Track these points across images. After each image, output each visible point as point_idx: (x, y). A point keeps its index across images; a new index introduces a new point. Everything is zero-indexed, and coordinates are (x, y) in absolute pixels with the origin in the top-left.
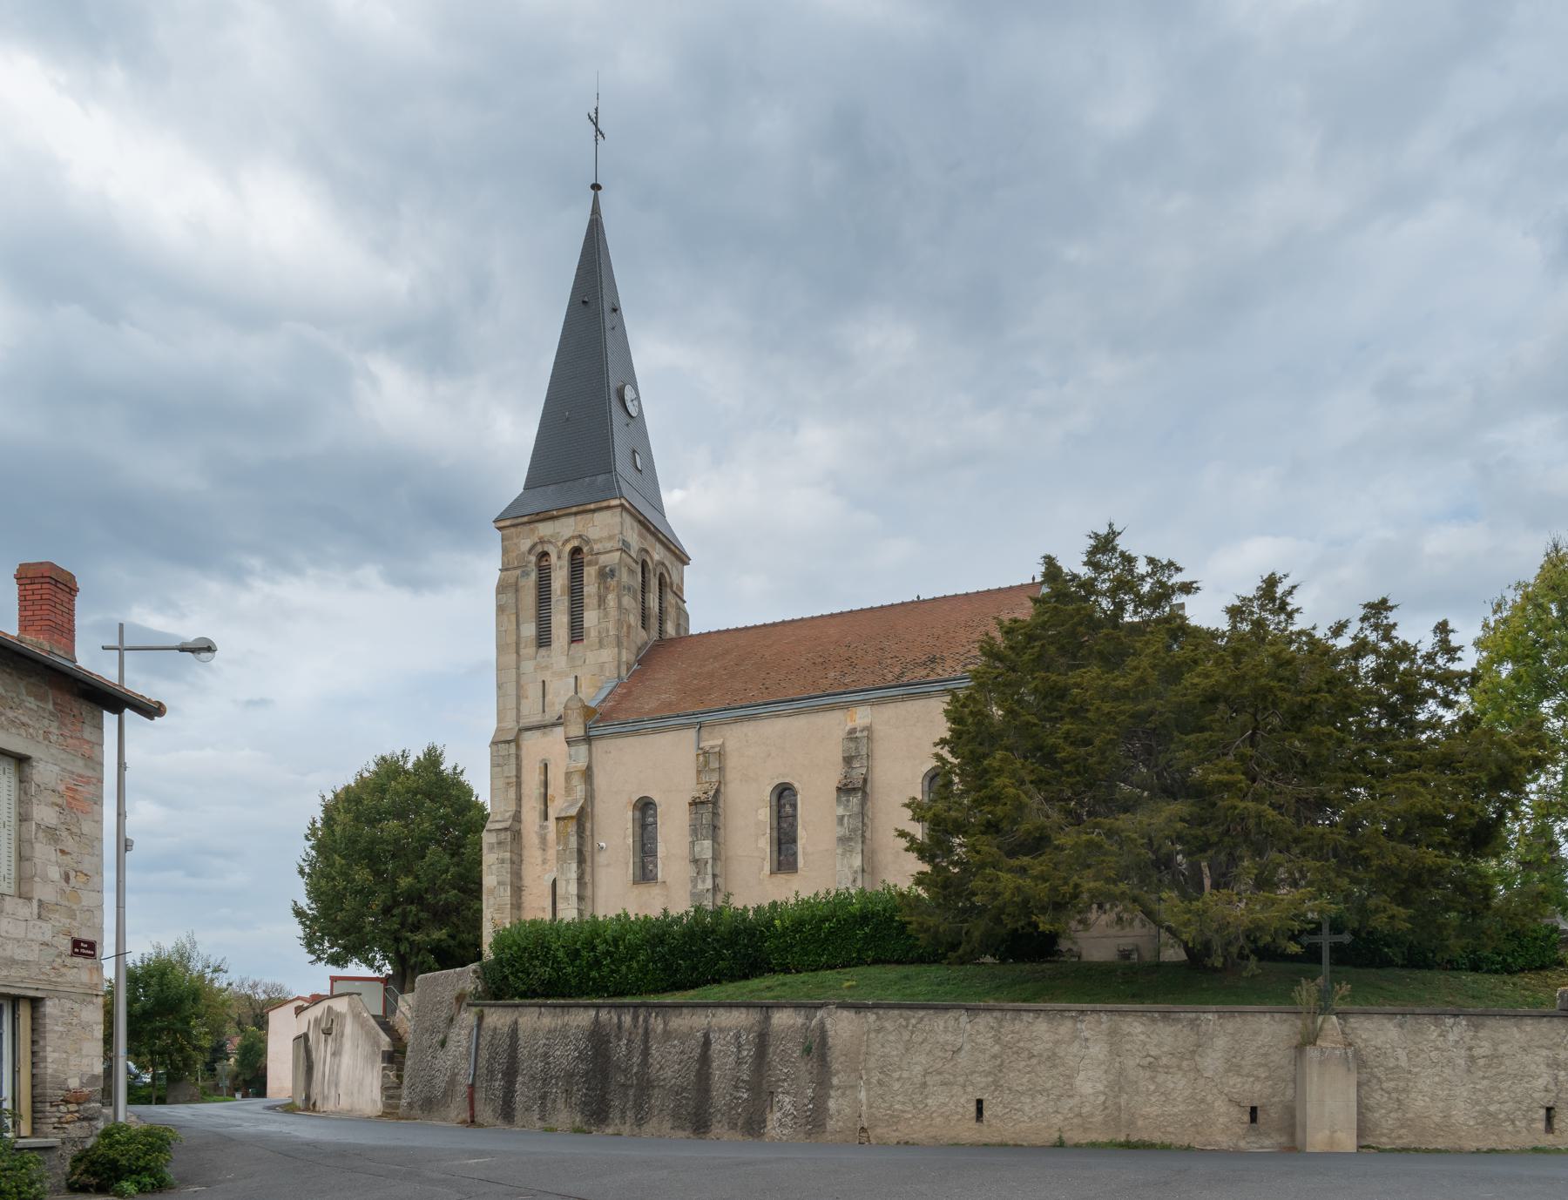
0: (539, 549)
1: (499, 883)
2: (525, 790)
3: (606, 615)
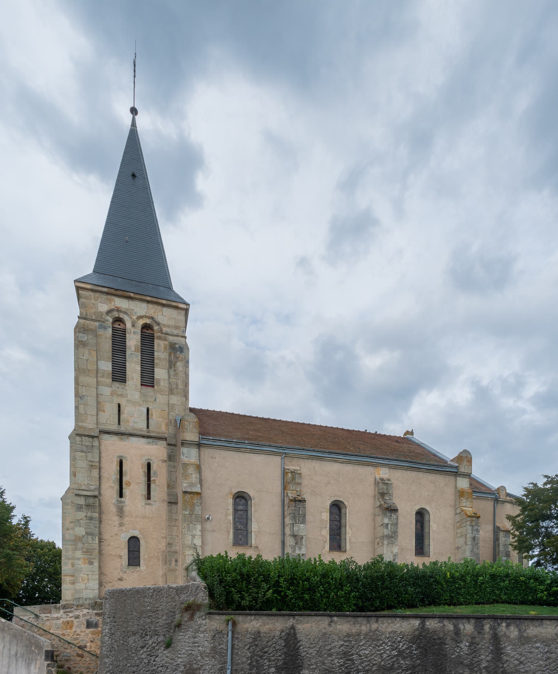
0: (116, 314)
1: (87, 533)
3: (176, 375)
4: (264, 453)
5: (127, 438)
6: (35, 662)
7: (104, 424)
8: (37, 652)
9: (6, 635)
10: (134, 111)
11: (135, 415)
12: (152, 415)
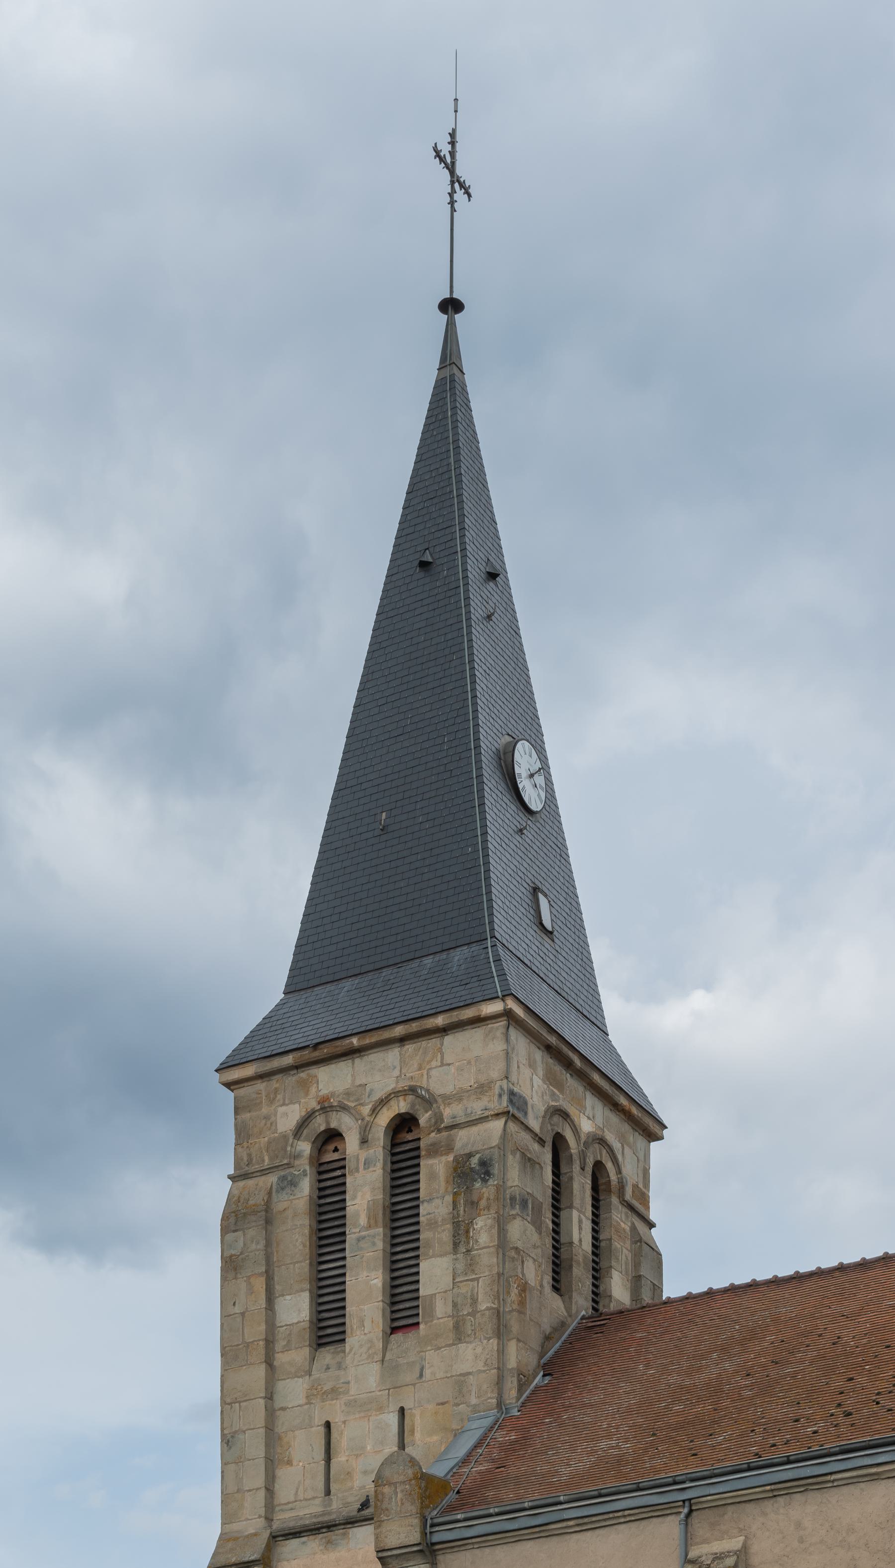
0: (319, 1124)
3: (471, 1266)
4: (622, 1520)
5: (344, 1534)
7: (290, 1506)
11: (369, 1448)
12: (412, 1432)
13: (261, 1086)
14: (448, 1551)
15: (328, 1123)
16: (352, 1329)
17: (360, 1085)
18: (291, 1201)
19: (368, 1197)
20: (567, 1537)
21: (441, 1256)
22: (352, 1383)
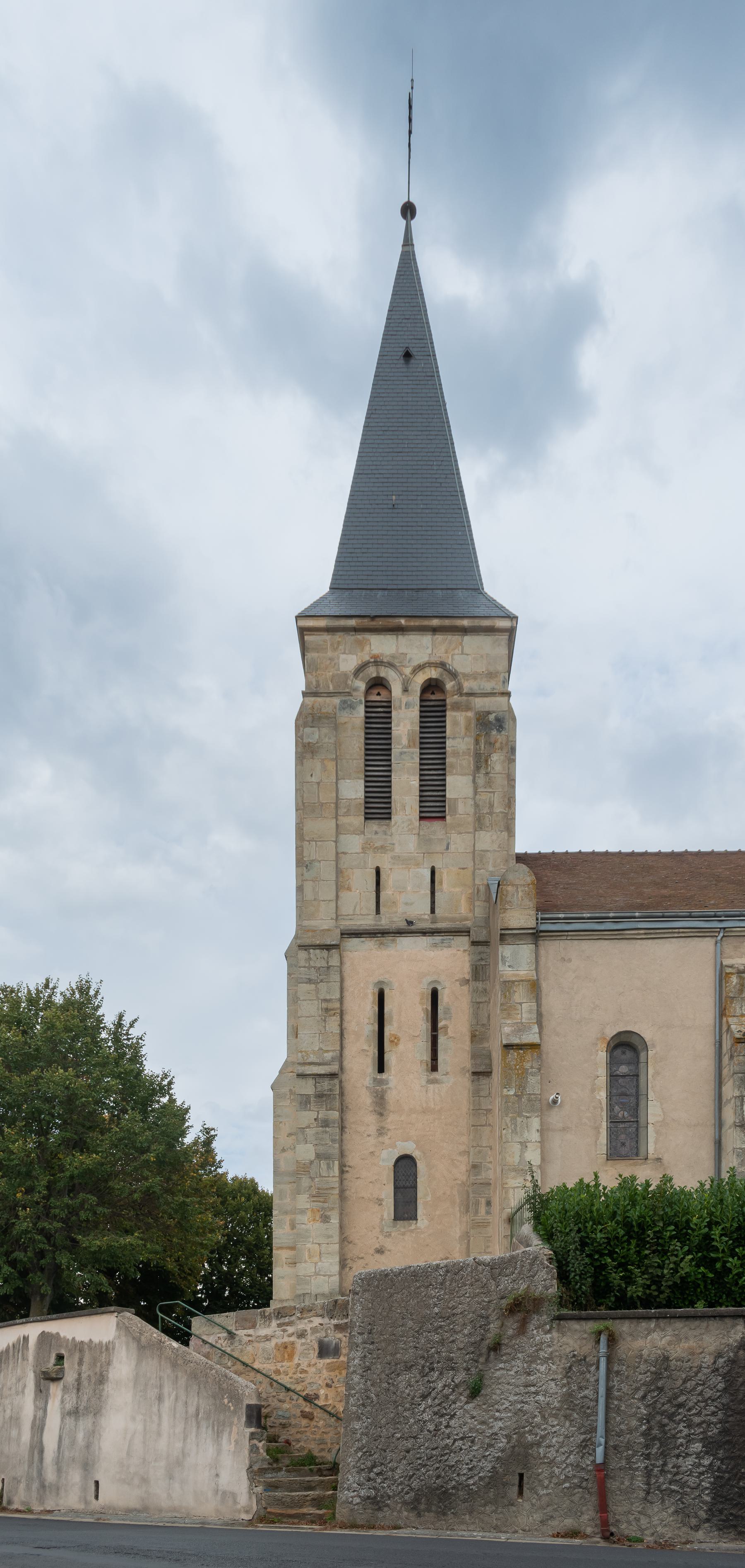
0: (372, 672)
1: (318, 1156)
2: (351, 1025)
3: (489, 783)
4: (676, 935)
5: (393, 940)
6: (228, 1429)
7: (350, 917)
8: (232, 1408)
9: (180, 1374)
10: (408, 211)
11: (409, 888)
12: (441, 883)
13: (326, 637)
14: (548, 939)
15: (378, 673)
16: (396, 810)
17: (402, 654)
18: (351, 718)
19: (409, 727)
20: (634, 941)
21: (462, 775)
22: (397, 845)
